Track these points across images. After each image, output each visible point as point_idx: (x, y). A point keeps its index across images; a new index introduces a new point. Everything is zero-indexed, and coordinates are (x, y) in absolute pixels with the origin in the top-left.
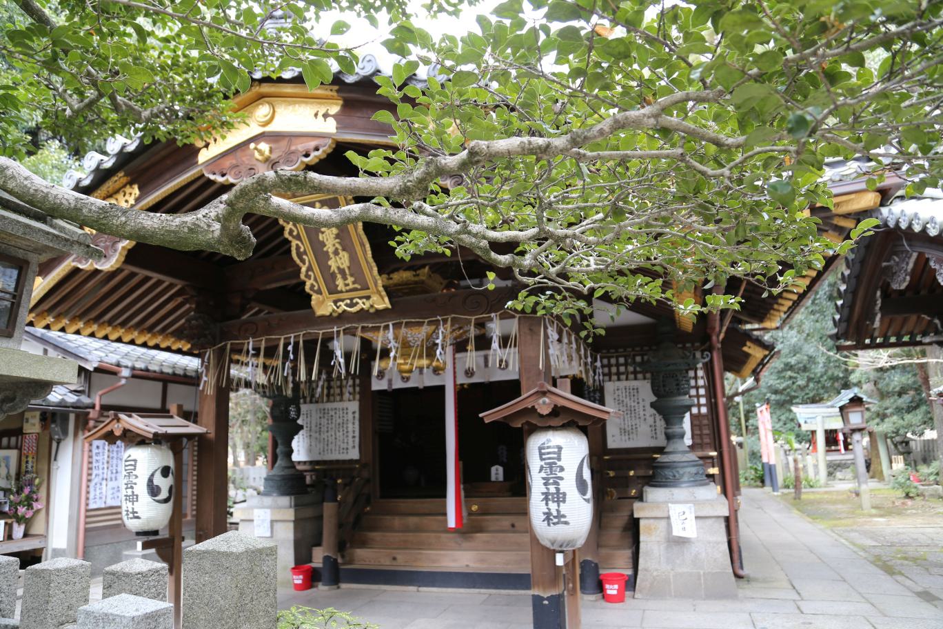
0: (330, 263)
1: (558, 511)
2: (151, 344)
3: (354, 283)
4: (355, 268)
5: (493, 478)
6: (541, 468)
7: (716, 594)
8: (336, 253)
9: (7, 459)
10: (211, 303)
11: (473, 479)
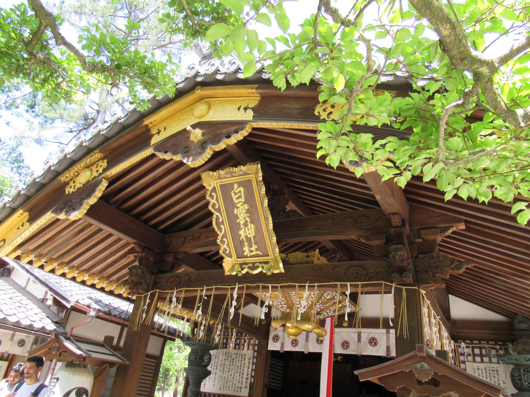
0: (240, 233)
2: (107, 289)
3: (257, 250)
8: (246, 224)
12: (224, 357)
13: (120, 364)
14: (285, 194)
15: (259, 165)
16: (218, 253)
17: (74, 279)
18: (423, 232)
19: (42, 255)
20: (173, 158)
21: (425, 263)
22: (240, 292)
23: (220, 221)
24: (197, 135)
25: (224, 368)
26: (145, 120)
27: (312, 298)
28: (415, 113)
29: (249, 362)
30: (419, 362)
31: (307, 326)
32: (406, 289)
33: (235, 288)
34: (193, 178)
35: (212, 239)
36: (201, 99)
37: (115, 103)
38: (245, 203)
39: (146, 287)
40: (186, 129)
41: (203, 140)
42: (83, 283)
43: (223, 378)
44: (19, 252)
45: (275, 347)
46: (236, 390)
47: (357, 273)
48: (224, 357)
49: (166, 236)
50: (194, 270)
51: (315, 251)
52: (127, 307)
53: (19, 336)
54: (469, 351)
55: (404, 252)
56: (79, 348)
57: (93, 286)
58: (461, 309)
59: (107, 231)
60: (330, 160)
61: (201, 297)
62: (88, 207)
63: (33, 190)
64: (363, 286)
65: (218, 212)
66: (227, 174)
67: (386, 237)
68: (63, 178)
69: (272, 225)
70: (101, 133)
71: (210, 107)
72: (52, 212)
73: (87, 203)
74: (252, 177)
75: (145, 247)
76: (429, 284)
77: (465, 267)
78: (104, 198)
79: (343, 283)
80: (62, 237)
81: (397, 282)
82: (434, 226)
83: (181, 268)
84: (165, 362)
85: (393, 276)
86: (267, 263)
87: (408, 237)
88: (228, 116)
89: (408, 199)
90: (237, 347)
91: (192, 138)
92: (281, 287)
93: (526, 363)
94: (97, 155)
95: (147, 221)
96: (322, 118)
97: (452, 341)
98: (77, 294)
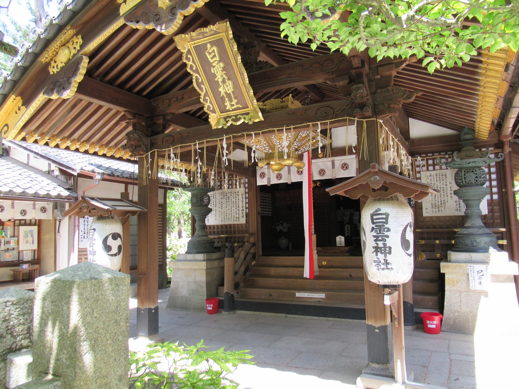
0: (220, 90)
1: (386, 261)
3: (237, 103)
4: (237, 93)
5: (338, 245)
6: (373, 229)
9: (31, 232)
10: (144, 124)
11: (324, 243)
12: (221, 197)
14: (255, 46)
15: (228, 23)
17: (77, 150)
18: (380, 69)
19: (44, 133)
27: (290, 138)
30: (373, 176)
33: (223, 139)
35: (195, 98)
38: (220, 61)
42: (86, 152)
43: (223, 213)
44: (23, 134)
45: (263, 182)
48: (221, 197)
52: (133, 168)
53: (40, 204)
54: (424, 162)
56: (105, 205)
57: (95, 154)
58: (419, 129)
60: (291, 39)
61: (195, 151)
63: (18, 75)
65: (196, 73)
68: (44, 59)
70: (68, 8)
72: (44, 94)
73: (75, 82)
74: (223, 35)
75: (136, 114)
76: (385, 114)
77: (415, 96)
78: (89, 73)
80: (58, 115)
81: (359, 116)
86: (247, 114)
87: (367, 75)
90: (230, 187)
92: (262, 133)
93: (467, 165)
94: (69, 32)
95: (130, 89)
97: (410, 157)
98: (79, 162)
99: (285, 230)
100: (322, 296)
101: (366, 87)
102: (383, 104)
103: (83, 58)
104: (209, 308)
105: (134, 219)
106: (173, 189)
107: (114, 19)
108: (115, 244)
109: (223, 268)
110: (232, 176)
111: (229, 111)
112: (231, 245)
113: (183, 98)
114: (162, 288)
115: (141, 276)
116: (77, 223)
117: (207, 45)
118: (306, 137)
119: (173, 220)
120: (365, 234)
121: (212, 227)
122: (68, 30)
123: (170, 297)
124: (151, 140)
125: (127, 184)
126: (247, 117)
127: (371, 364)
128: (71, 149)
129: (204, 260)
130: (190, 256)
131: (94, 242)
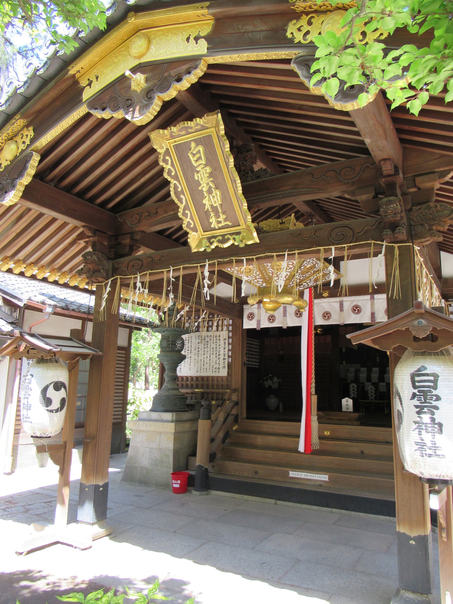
0: (204, 202)
3: (225, 220)
4: (227, 206)
5: (344, 409)
6: (414, 396)
7: (22, 361)
8: (210, 191)
12: (198, 341)
13: (93, 355)
14: (251, 150)
15: (220, 115)
16: (181, 228)
17: (22, 274)
18: (418, 179)
20: (114, 115)
21: (420, 215)
22: (212, 270)
23: (179, 190)
24: (139, 81)
25: (199, 351)
26: (69, 68)
27: (290, 268)
28: (440, 7)
29: (225, 343)
30: (416, 319)
31: (287, 299)
32: (398, 247)
33: (205, 265)
34: (137, 141)
35: (172, 213)
36: (137, 31)
37: (17, 54)
38: (206, 165)
39: (105, 274)
40: (124, 74)
41: (147, 88)
42: (33, 277)
43: (199, 361)
46: (214, 371)
47: (342, 234)
48: (198, 341)
49: (117, 215)
50: (154, 251)
51: (290, 215)
52: (88, 300)
55: (397, 205)
56: (47, 344)
57: (45, 280)
59: (49, 216)
62: (22, 189)
64: (350, 248)
66: (181, 131)
67: (375, 190)
69: (241, 188)
70: (18, 92)
71: (149, 42)
73: (21, 184)
75: (96, 230)
76: (425, 238)
79: (327, 247)
81: (389, 240)
82: (433, 170)
83: (140, 251)
84: (134, 354)
85: (385, 233)
86: (238, 233)
87: (401, 187)
88: (174, 51)
89: (402, 141)
91: (134, 86)
92: (257, 259)
94: (18, 123)
95: (92, 200)
96: (296, 41)
98: (27, 290)
99: (275, 386)
100: (324, 477)
101: (400, 201)
102: (422, 225)
103: (32, 155)
104: (175, 486)
105: (85, 364)
106: (140, 329)
107: (74, 107)
108: (57, 397)
109: (196, 432)
110: (213, 316)
111: (214, 229)
112: (207, 403)
113: (157, 212)
114: (118, 453)
115: (88, 440)
116: (19, 366)
117: (190, 144)
118: (311, 268)
119: (140, 367)
120: (401, 401)
121: (185, 378)
122: (18, 119)
123: (127, 467)
124: (113, 263)
125: (84, 321)
126: (237, 237)
127: (402, 592)
128: (15, 272)
129: (172, 421)
130: (155, 415)
131: (29, 393)
